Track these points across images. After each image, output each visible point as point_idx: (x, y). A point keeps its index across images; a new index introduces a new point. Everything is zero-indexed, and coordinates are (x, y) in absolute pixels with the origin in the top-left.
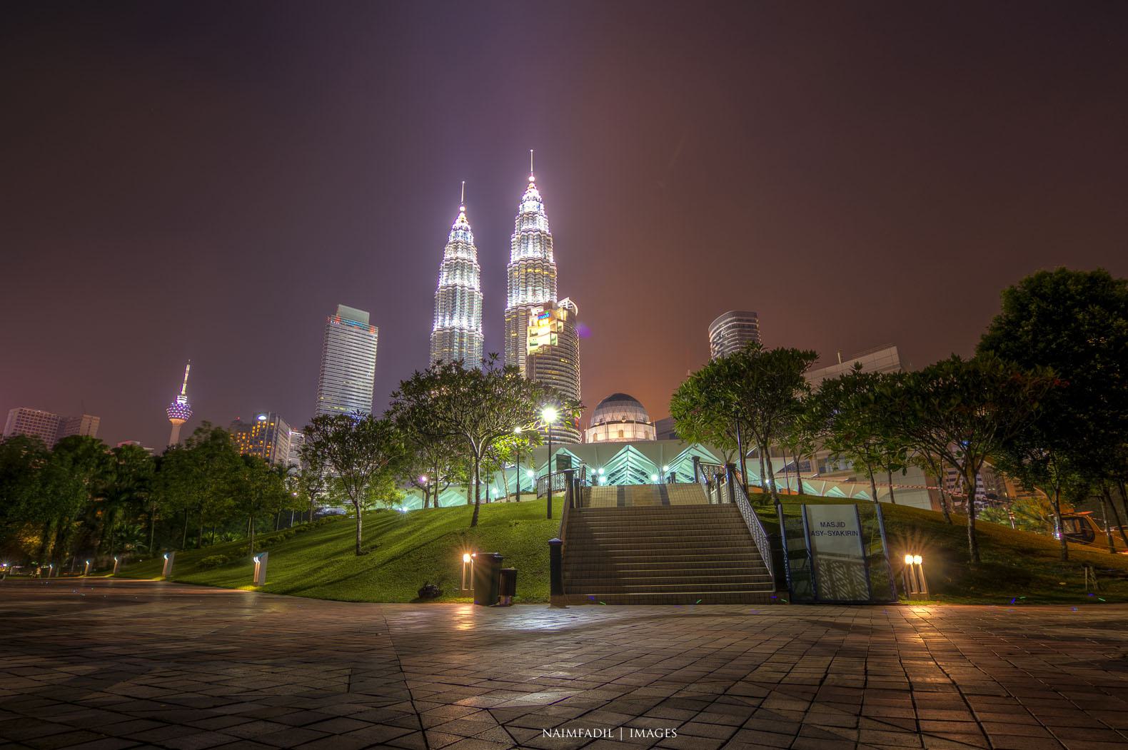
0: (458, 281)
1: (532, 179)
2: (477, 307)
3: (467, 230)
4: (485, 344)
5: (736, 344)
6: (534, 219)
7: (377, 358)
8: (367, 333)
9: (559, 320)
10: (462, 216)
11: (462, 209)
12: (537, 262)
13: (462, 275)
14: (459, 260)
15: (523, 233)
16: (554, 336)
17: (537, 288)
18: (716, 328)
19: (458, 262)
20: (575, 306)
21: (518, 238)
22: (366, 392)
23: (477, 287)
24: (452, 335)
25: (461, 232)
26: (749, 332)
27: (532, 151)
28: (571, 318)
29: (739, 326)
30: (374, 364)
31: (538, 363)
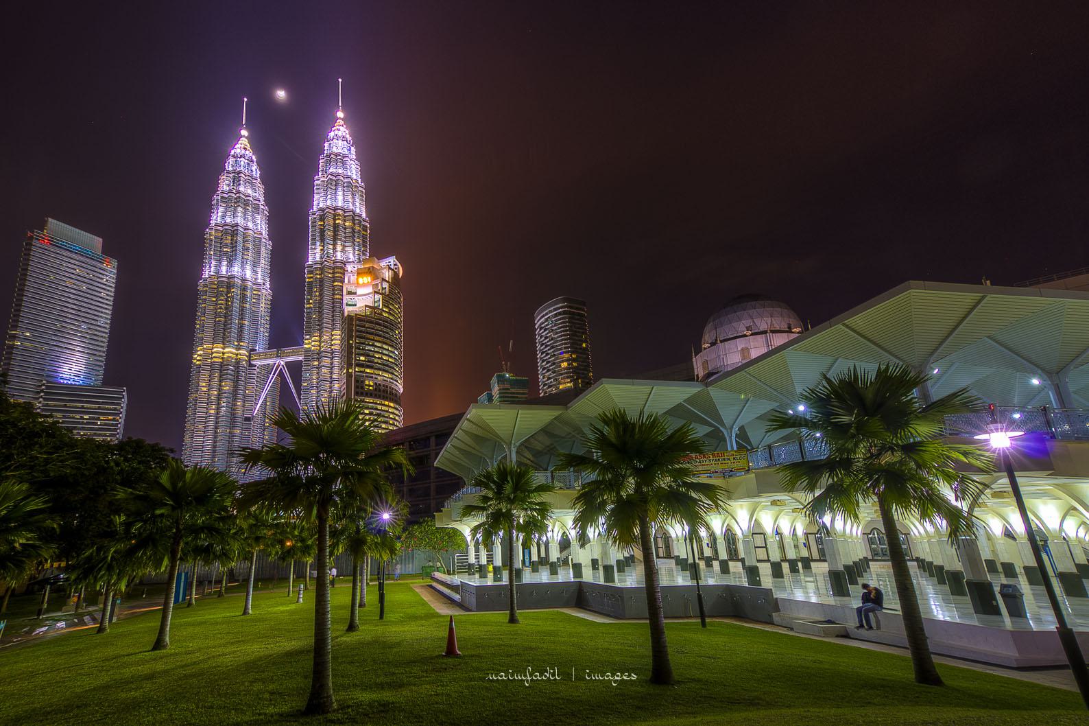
0: (239, 220)
1: (340, 114)
2: (264, 254)
3: (252, 161)
4: (275, 306)
5: (566, 331)
6: (344, 164)
7: (114, 301)
8: (100, 265)
9: (384, 280)
10: (244, 142)
11: (244, 133)
12: (347, 214)
13: (245, 214)
14: (241, 195)
15: (330, 176)
16: (378, 297)
17: (347, 244)
18: (544, 313)
19: (239, 197)
20: (400, 266)
21: (324, 181)
22: (97, 343)
23: (265, 233)
24: (230, 286)
25: (243, 162)
26: (578, 319)
27: (340, 80)
28: (395, 280)
29: (569, 313)
30: (112, 299)
31: (358, 331)
